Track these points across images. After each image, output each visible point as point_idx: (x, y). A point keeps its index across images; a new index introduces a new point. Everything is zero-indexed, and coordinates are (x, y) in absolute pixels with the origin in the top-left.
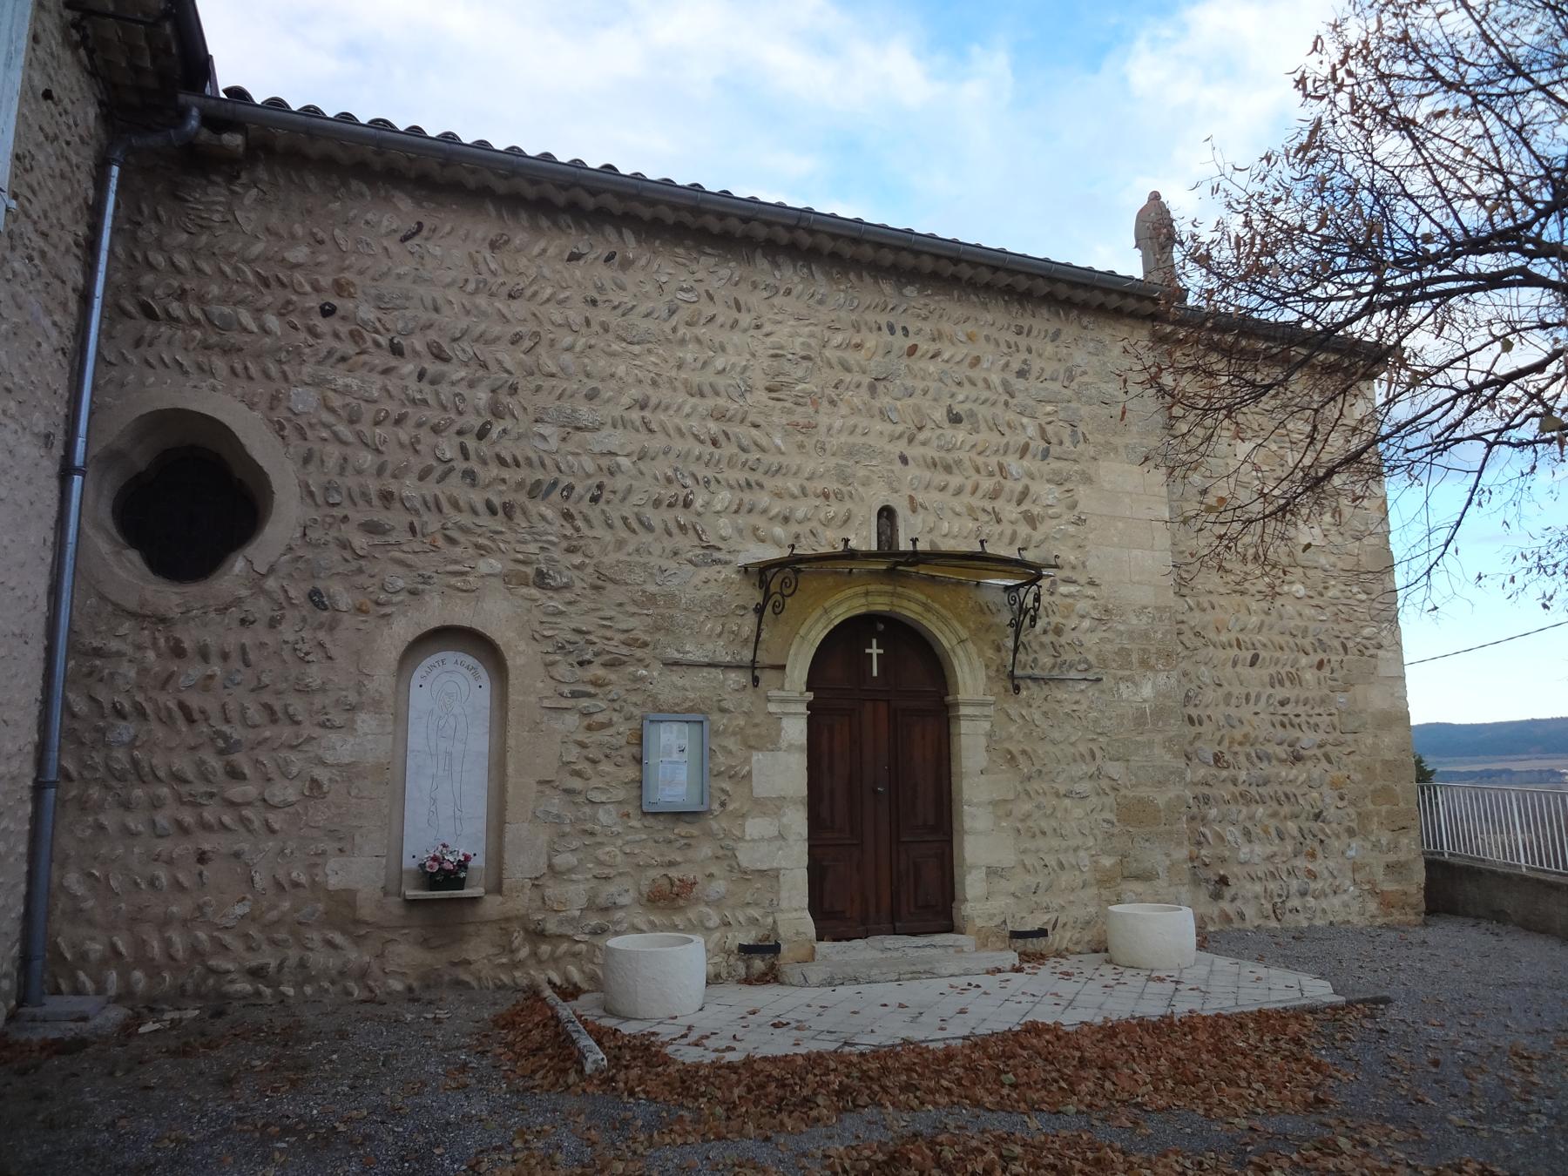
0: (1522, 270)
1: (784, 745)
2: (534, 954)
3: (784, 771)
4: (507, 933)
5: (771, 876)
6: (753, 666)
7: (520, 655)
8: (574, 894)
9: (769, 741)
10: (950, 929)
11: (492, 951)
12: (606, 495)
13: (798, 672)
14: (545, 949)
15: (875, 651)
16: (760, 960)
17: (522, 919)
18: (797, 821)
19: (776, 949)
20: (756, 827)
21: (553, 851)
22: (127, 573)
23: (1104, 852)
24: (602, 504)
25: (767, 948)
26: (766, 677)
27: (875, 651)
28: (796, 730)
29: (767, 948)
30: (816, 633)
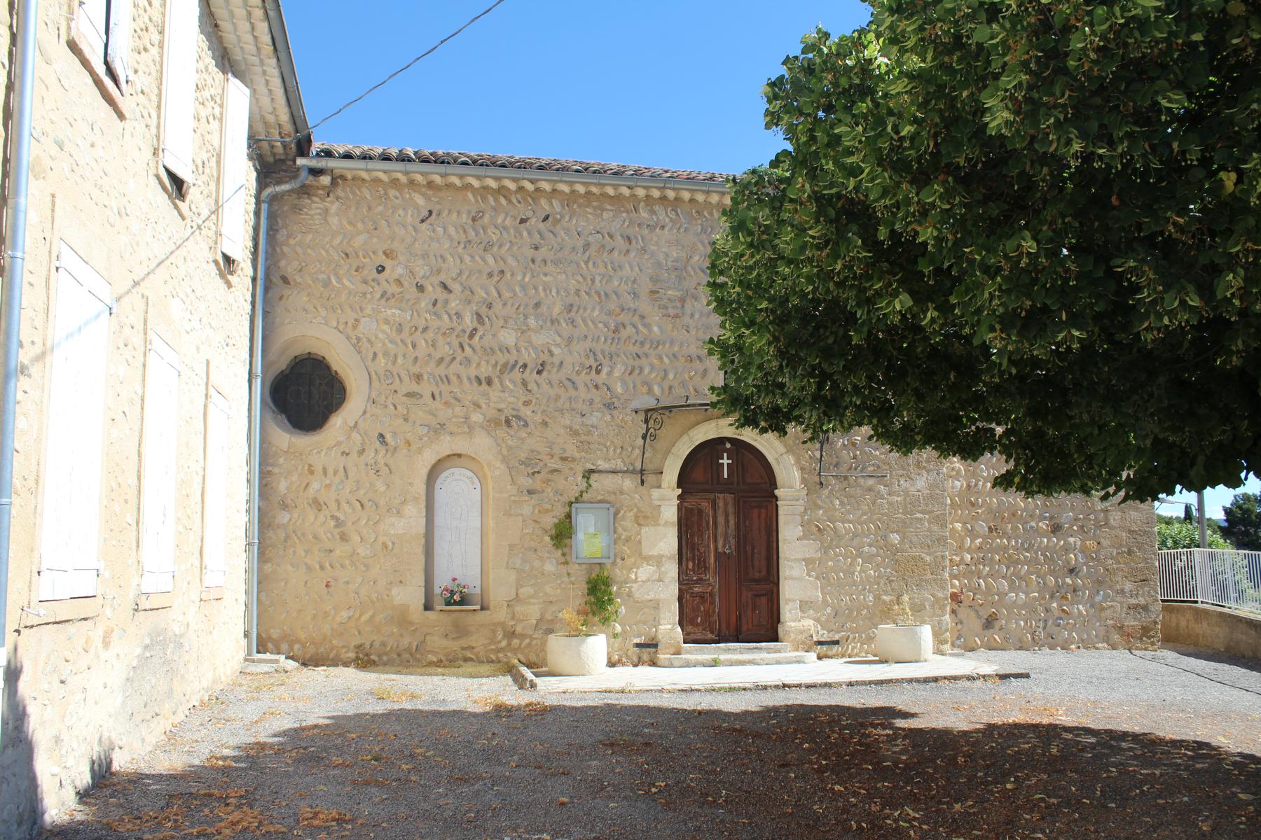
0: (1077, 735)
1: (662, 522)
2: (509, 644)
3: (666, 541)
4: (494, 632)
5: (656, 605)
6: (642, 472)
7: (460, 445)
8: (532, 611)
9: (646, 517)
10: (775, 639)
11: (486, 642)
12: (548, 367)
13: (671, 474)
14: (516, 642)
15: (725, 461)
16: (648, 652)
17: (503, 624)
18: (672, 570)
19: (656, 646)
20: (645, 572)
21: (519, 586)
22: (284, 438)
23: (886, 593)
24: (545, 373)
25: (652, 645)
26: (650, 479)
27: (725, 461)
28: (670, 512)
29: (652, 645)
30: (683, 449)
